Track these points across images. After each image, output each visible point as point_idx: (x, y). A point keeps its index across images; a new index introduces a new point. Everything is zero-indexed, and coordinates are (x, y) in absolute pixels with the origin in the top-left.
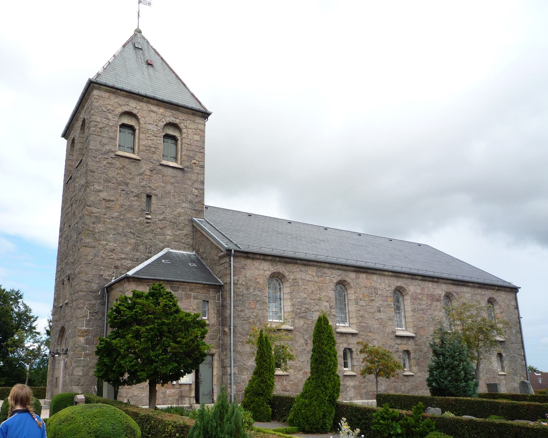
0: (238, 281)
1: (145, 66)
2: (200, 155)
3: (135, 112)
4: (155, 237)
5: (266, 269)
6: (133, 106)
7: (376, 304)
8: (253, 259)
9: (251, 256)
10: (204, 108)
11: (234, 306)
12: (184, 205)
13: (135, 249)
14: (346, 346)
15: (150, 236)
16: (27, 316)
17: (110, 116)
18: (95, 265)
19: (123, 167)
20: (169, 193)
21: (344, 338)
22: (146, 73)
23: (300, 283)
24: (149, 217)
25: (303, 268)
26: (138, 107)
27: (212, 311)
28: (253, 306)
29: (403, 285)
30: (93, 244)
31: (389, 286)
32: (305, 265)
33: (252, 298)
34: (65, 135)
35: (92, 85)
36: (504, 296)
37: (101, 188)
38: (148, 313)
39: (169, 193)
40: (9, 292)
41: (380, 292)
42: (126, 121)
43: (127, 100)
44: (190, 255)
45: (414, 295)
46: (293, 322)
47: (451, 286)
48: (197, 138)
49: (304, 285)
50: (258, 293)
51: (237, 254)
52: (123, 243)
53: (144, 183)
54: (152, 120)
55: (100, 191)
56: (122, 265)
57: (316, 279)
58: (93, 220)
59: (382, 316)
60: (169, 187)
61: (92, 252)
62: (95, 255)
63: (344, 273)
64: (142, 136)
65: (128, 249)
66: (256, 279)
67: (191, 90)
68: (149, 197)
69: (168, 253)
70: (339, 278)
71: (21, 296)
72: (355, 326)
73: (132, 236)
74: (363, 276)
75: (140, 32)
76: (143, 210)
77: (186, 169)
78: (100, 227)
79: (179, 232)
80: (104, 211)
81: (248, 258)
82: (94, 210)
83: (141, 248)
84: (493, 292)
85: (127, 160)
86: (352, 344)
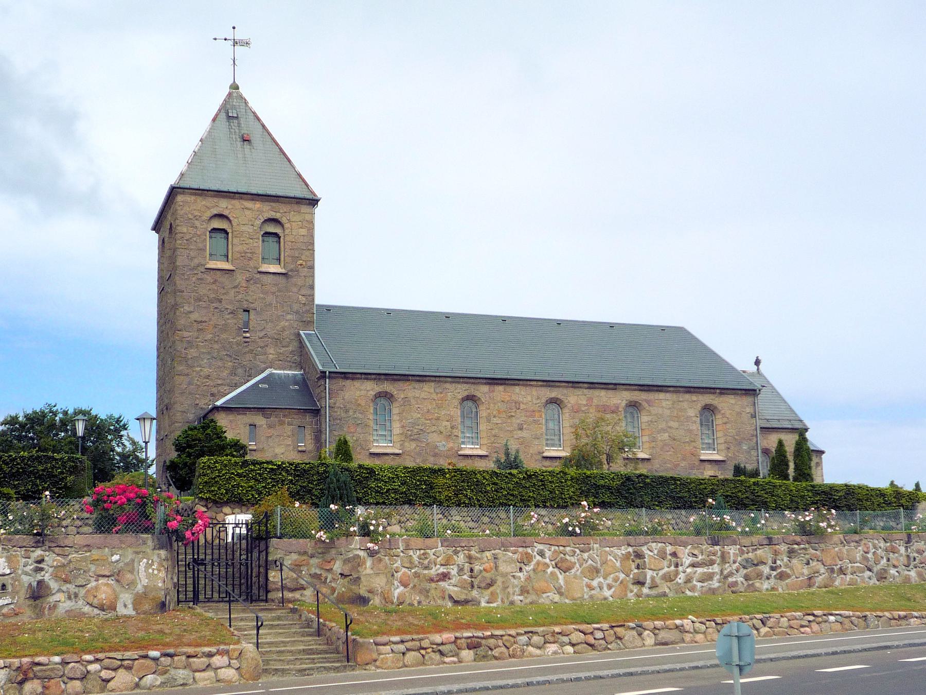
1: (239, 144)
2: (307, 253)
3: (226, 213)
4: (255, 359)
5: (370, 388)
6: (223, 205)
7: (516, 421)
8: (353, 379)
9: (350, 376)
10: (312, 193)
11: (330, 431)
12: (289, 317)
13: (233, 373)
15: (249, 357)
16: (137, 458)
17: (197, 223)
18: (190, 393)
19: (215, 281)
20: (270, 304)
22: (240, 156)
24: (248, 335)
25: (417, 385)
26: (230, 207)
27: (308, 437)
29: (559, 396)
30: (186, 372)
31: (538, 398)
32: (419, 381)
34: (157, 227)
35: (173, 192)
36: (733, 401)
38: (194, 440)
39: (270, 304)
40: (106, 420)
41: (522, 406)
42: (217, 224)
43: (216, 200)
44: (295, 375)
45: (576, 407)
46: (401, 445)
47: (637, 393)
48: (303, 232)
51: (333, 375)
52: (219, 367)
54: (247, 219)
55: (191, 312)
56: (219, 392)
58: (185, 345)
59: (524, 434)
60: (270, 299)
61: (187, 379)
62: (190, 384)
63: (473, 387)
64: (236, 241)
65: (225, 373)
66: (357, 400)
67: (299, 168)
69: (271, 375)
70: (466, 393)
71: (124, 425)
72: (485, 447)
73: (228, 359)
75: (237, 88)
76: (240, 329)
78: (193, 352)
79: (284, 349)
80: (196, 334)
81: (347, 378)
82: (186, 334)
83: (240, 371)
84: (712, 396)
85: (218, 272)
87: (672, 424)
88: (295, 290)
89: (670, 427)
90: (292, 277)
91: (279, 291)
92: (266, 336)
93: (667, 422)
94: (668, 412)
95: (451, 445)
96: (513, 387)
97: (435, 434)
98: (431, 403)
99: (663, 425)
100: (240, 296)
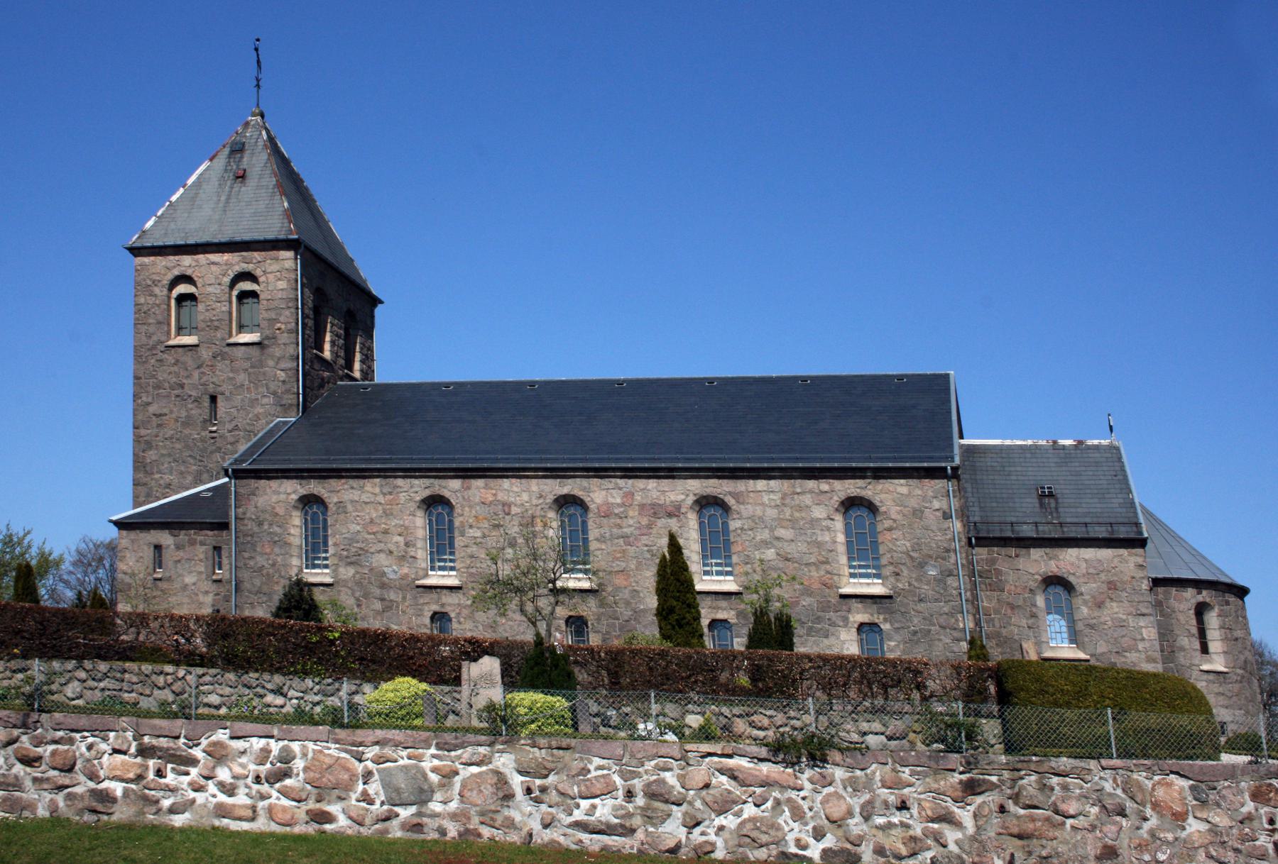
0: (244, 514)
3: (189, 272)
8: (269, 478)
12: (265, 400)
14: (435, 608)
19: (177, 362)
21: (434, 595)
23: (350, 508)
28: (268, 550)
30: (145, 480)
31: (541, 496)
33: (266, 538)
36: (904, 490)
37: (150, 400)
41: (514, 510)
49: (356, 510)
50: (276, 529)
52: (182, 473)
53: (205, 378)
55: (149, 404)
57: (381, 499)
63: (436, 482)
68: (213, 399)
70: (427, 493)
74: (480, 483)
77: (266, 342)
80: (155, 431)
81: (261, 478)
84: (860, 482)
86: (450, 605)
87: (781, 532)
88: (271, 363)
89: (778, 539)
90: (268, 346)
91: (252, 367)
92: (236, 428)
93: (772, 530)
94: (772, 513)
95: (406, 570)
96: (500, 481)
97: (382, 556)
98: (376, 510)
99: (765, 535)
100: (205, 378)
